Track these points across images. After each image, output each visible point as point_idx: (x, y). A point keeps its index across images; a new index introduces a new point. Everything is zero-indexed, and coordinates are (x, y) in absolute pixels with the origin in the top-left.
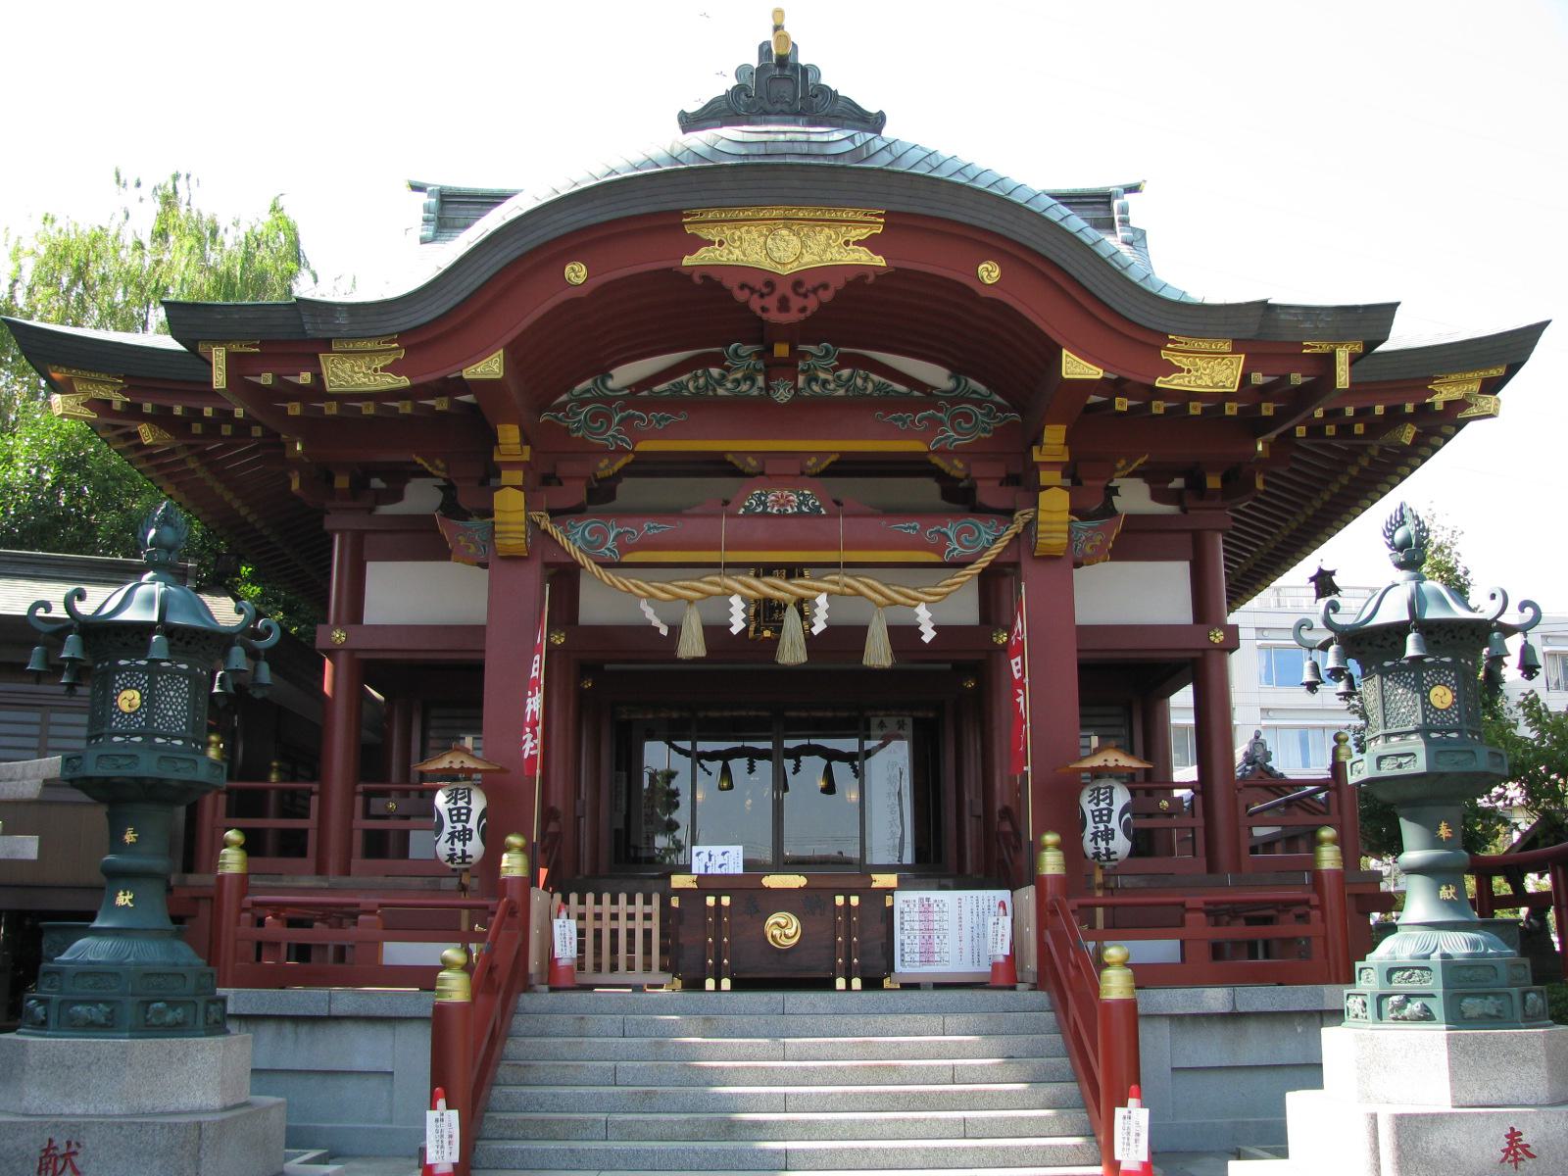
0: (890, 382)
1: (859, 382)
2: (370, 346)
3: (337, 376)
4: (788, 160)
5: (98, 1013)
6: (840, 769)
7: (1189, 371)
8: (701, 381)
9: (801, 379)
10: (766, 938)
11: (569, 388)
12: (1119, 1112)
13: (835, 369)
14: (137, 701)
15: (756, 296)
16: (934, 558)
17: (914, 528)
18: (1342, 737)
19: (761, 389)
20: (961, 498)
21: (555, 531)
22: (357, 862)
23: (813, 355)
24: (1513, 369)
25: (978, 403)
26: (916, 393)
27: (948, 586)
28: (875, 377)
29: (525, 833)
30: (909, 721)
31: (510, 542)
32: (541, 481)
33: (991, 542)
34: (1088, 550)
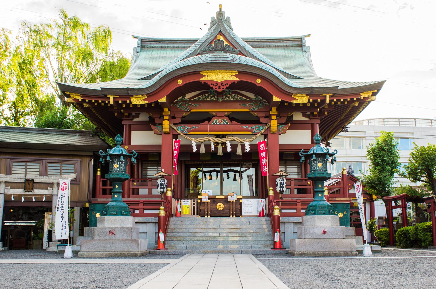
0: (242, 97)
1: (236, 97)
2: (140, 96)
3: (134, 101)
4: (220, 61)
5: (115, 213)
6: (237, 175)
7: (298, 99)
8: (204, 97)
9: (224, 96)
10: (217, 209)
11: (177, 99)
12: (275, 234)
13: (231, 94)
14: (117, 166)
15: (214, 86)
16: (251, 133)
17: (247, 127)
18: (344, 169)
19: (216, 99)
20: (257, 122)
21: (175, 128)
22: (131, 195)
23: (227, 91)
24: (378, 91)
25: (260, 101)
26: (248, 99)
27: (253, 138)
28: (239, 96)
29: (171, 188)
30: (251, 164)
31: (166, 131)
32: (172, 117)
33: (262, 129)
34: (282, 131)
